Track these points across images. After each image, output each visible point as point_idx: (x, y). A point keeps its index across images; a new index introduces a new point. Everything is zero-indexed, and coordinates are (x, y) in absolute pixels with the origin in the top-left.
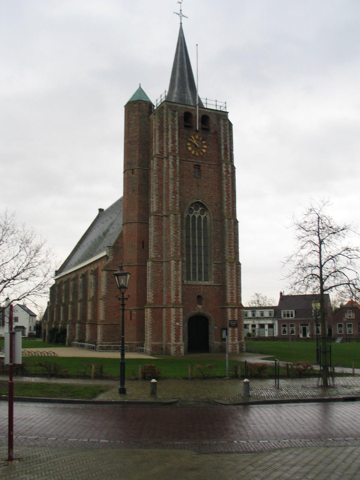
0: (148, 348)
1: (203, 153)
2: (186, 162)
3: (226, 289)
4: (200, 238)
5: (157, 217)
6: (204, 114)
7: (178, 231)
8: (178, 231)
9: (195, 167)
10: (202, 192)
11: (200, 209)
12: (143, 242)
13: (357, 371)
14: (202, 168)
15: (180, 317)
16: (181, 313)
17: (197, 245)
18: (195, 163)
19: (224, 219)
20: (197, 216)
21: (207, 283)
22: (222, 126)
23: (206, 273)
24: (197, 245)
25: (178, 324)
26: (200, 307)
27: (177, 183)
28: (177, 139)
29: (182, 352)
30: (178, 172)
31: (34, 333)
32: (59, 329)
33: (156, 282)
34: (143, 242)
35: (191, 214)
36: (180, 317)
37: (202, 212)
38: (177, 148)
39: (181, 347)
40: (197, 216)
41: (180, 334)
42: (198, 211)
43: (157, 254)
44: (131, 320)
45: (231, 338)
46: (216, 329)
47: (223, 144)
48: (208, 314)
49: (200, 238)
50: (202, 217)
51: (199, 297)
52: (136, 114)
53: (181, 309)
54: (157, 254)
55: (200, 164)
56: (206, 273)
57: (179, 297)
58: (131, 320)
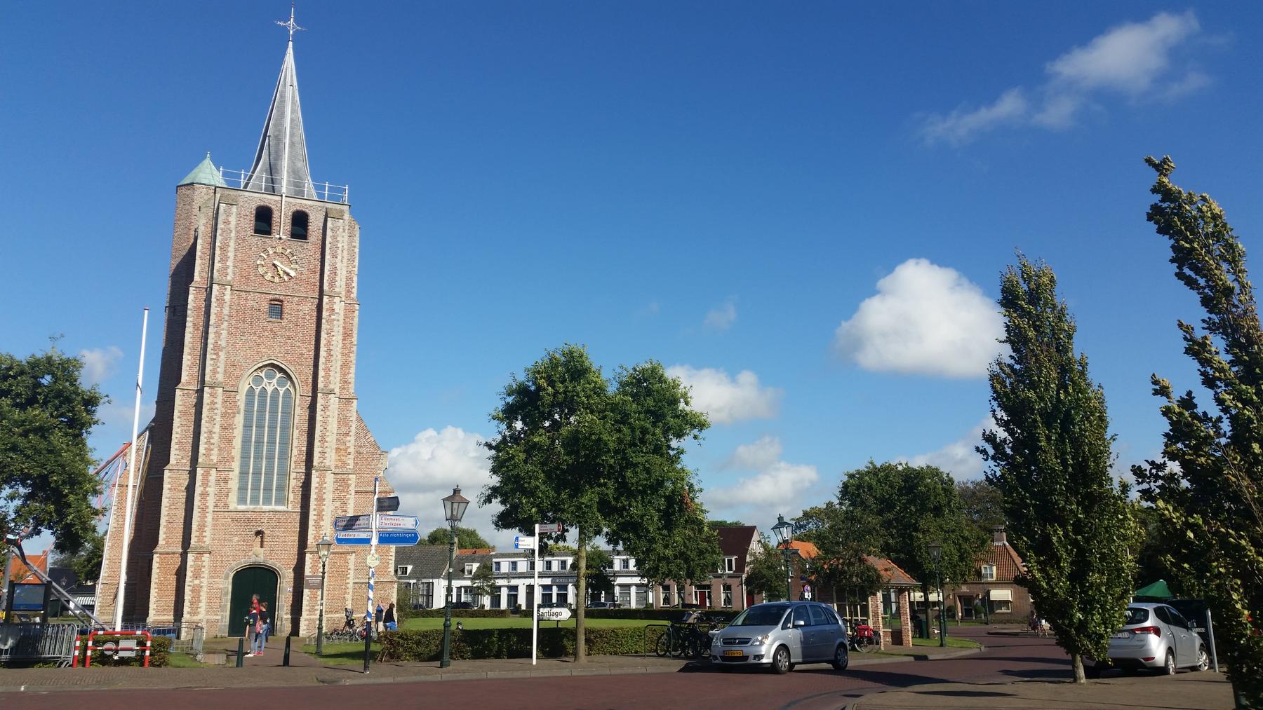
4: (273, 428)
20: (270, 390)
25: (197, 582)
28: (231, 254)
37: (280, 384)
40: (270, 390)
51: (259, 533)
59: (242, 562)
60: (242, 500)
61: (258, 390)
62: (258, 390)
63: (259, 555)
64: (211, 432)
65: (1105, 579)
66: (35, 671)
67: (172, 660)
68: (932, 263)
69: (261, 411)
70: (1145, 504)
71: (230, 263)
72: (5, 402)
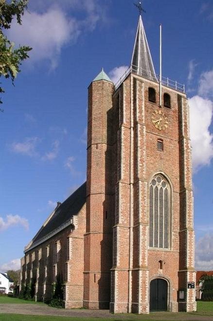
0: (69, 301)
3: (26, 299)
6: (166, 92)
7: (145, 198)
10: (164, 165)
12: (107, 212)
13: (1, 289)
14: (164, 142)
16: (147, 276)
17: (159, 215)
19: (185, 191)
20: (159, 188)
21: (166, 249)
23: (166, 242)
24: (159, 215)
26: (161, 271)
27: (144, 151)
31: (11, 293)
34: (107, 212)
37: (164, 184)
38: (144, 118)
40: (159, 188)
42: (161, 183)
43: (123, 220)
48: (167, 277)
51: (160, 262)
52: (100, 92)
53: (148, 272)
54: (123, 220)
55: (163, 138)
56: (166, 242)
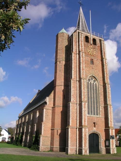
1: (94, 54)
2: (87, 57)
3: (17, 145)
4: (94, 94)
5: (74, 81)
6: (94, 38)
7: (85, 88)
8: (85, 88)
9: (91, 60)
11: (94, 79)
15: (87, 133)
16: (87, 131)
17: (92, 97)
18: (91, 58)
20: (92, 83)
21: (97, 116)
22: (24, 150)
24: (92, 97)
26: (95, 128)
28: (83, 45)
29: (87, 153)
30: (84, 60)
31: (9, 141)
32: (61, 147)
33: (73, 114)
35: (89, 81)
36: (87, 133)
37: (94, 81)
38: (83, 49)
39: (87, 150)
40: (92, 83)
41: (87, 143)
42: (93, 81)
43: (73, 100)
44: (57, 135)
45: (112, 145)
46: (102, 140)
47: (103, 51)
49: (94, 94)
50: (95, 83)
51: (94, 123)
53: (87, 129)
55: (93, 59)
57: (86, 122)
58: (57, 135)
59: (91, 132)
60: (89, 113)
61: (89, 82)
62: (89, 82)
63: (94, 130)
64: (111, 121)
65: (11, 24)
66: (52, 152)
67: (51, 109)
68: (71, 27)
69: (91, 89)
70: (2, 19)
71: (83, 47)
72: (1, 23)
